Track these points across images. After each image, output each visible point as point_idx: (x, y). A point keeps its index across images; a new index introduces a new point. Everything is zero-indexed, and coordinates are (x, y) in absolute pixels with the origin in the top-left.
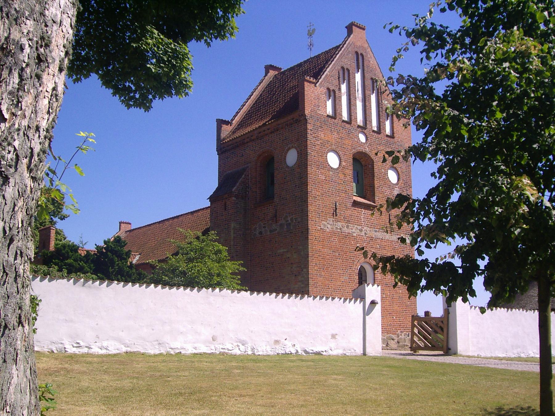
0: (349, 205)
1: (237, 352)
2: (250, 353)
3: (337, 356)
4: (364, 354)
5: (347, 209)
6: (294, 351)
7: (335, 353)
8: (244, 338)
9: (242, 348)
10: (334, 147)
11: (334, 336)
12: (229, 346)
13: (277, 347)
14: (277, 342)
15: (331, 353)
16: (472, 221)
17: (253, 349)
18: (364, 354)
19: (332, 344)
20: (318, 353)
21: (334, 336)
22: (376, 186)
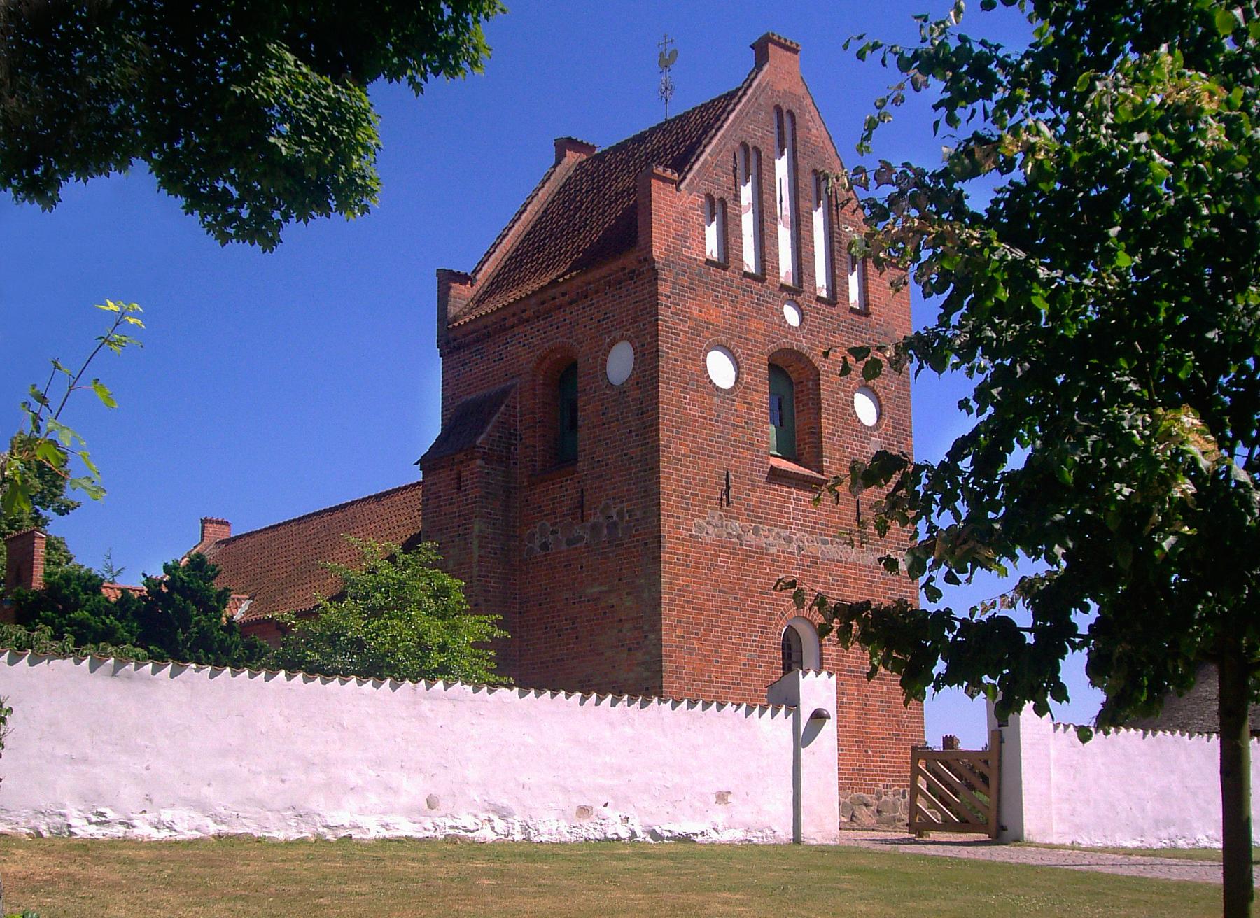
0: (760, 478)
1: (487, 834)
2: (518, 837)
3: (731, 845)
4: (797, 839)
6: (624, 834)
7: (725, 837)
8: (504, 801)
9: (500, 825)
11: (722, 797)
12: (469, 822)
14: (584, 811)
15: (715, 837)
18: (797, 839)
20: (685, 839)
21: (722, 797)
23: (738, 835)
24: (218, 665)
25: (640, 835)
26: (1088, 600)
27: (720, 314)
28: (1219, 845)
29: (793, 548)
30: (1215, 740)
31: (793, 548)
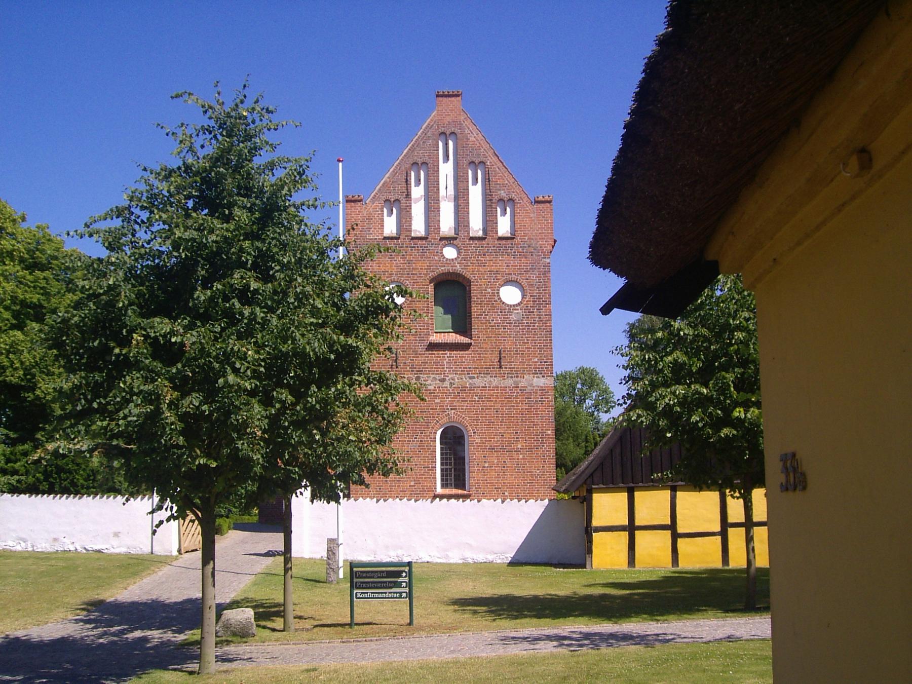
0: (421, 349)
1: (19, 548)
2: (30, 549)
3: (119, 554)
4: (152, 553)
5: (417, 354)
6: (72, 548)
7: (117, 551)
8: (23, 536)
9: (23, 544)
10: (394, 277)
11: (116, 535)
12: (11, 543)
13: (56, 544)
14: (55, 540)
15: (112, 550)
16: (705, 391)
17: (33, 546)
18: (152, 553)
19: (115, 542)
20: (99, 551)
21: (116, 535)
22: (474, 315)
23: (123, 550)
24: (37, 494)
25: (79, 549)
26: (395, 210)
27: (503, 263)
28: (769, 632)
29: (447, 384)
30: (717, 493)
31: (447, 384)
